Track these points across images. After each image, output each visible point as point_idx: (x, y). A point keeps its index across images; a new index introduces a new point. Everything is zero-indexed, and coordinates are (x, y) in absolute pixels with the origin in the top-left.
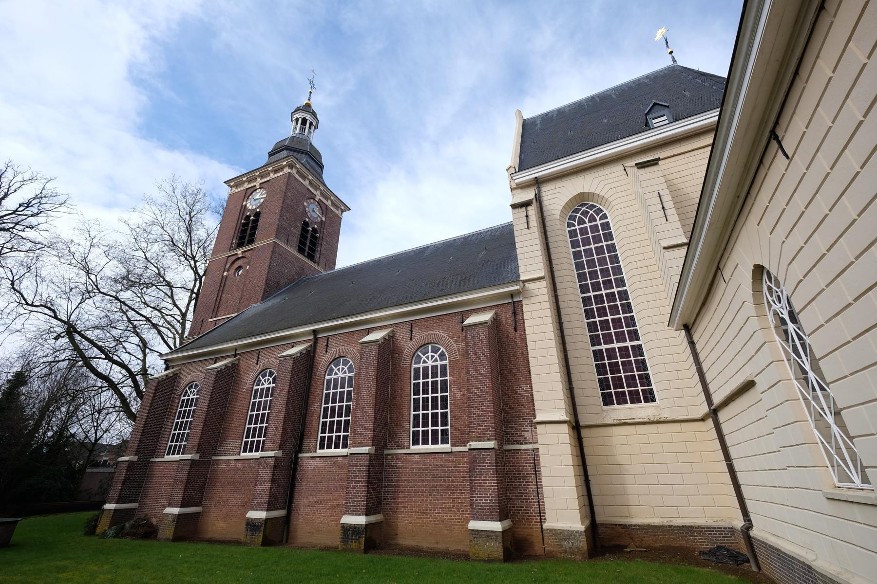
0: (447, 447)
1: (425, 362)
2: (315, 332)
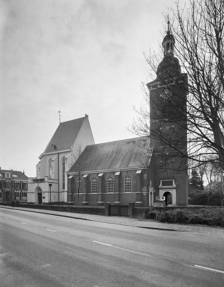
0: (131, 192)
1: (127, 178)
2: (121, 170)
